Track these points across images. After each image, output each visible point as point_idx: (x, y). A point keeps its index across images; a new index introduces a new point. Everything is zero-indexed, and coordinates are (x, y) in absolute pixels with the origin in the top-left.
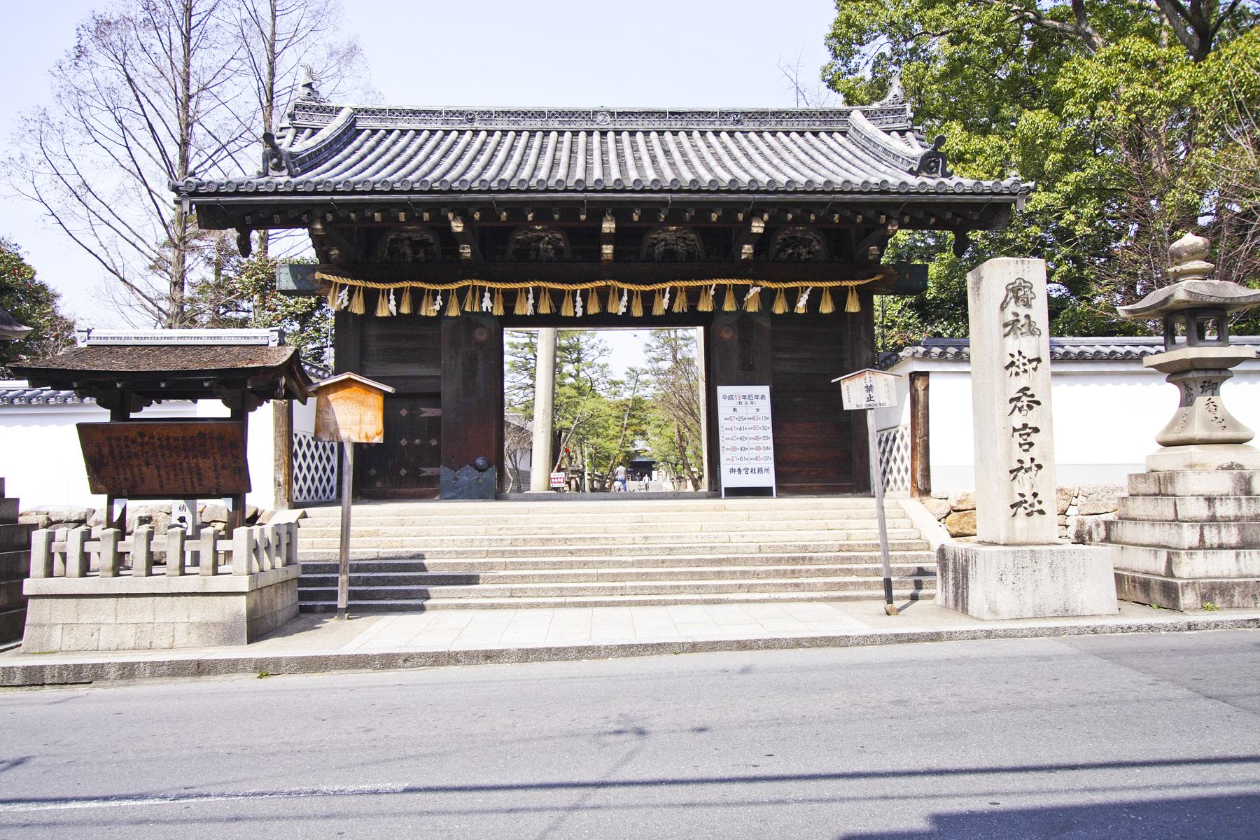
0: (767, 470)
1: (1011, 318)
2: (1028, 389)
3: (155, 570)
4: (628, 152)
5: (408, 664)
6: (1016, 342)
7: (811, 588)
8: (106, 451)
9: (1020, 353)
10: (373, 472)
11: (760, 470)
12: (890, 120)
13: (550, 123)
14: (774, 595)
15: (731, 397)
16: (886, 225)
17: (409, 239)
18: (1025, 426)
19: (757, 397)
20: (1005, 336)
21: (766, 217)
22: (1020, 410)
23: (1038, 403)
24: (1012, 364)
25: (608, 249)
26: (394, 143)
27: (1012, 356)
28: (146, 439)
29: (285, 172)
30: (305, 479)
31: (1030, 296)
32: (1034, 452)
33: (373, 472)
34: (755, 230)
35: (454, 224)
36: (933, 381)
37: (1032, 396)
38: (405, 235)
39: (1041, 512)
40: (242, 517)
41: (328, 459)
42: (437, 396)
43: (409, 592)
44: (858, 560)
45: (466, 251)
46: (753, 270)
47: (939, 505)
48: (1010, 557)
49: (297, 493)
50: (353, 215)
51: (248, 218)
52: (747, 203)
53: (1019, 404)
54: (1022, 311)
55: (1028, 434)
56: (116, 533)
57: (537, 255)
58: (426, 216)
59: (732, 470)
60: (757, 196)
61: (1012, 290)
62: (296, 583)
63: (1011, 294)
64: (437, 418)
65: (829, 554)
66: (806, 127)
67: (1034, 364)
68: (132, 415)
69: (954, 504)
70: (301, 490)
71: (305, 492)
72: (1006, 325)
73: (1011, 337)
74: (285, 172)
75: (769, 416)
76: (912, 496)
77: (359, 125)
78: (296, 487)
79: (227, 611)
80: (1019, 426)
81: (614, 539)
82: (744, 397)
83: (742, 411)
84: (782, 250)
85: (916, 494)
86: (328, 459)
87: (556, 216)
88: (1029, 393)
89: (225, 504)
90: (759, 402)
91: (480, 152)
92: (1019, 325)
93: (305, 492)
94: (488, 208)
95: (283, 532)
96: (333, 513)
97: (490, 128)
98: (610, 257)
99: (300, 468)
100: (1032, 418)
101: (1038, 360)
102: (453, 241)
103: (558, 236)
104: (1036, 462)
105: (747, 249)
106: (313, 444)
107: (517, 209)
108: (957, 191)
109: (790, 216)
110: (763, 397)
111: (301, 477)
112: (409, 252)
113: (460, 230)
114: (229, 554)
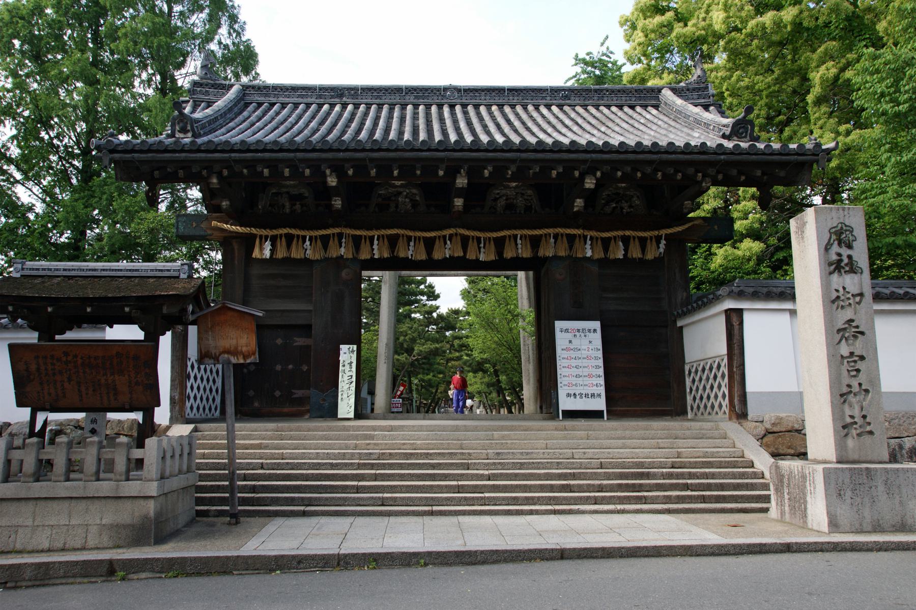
0: (599, 395)
1: (835, 258)
2: (852, 321)
3: (72, 476)
4: (475, 120)
5: (302, 566)
6: (841, 279)
7: (654, 500)
8: (33, 367)
9: (844, 288)
10: (251, 393)
11: (593, 395)
12: (695, 97)
13: (407, 97)
14: (619, 507)
15: (567, 331)
16: (701, 182)
17: (288, 193)
18: (852, 354)
19: (589, 331)
20: (831, 273)
21: (599, 174)
22: (846, 339)
23: (862, 333)
24: (838, 297)
25: (459, 202)
26: (278, 114)
27: (837, 291)
28: (69, 358)
29: (190, 135)
30: (195, 398)
31: (851, 238)
32: (862, 378)
33: (251, 393)
34: (587, 186)
35: (329, 179)
36: (747, 317)
37: (857, 327)
38: (284, 190)
39: (871, 433)
40: (148, 429)
41: (214, 381)
42: (308, 327)
43: (293, 499)
44: (647, 476)
45: (337, 203)
46: (587, 220)
47: (756, 427)
48: (848, 475)
49: (189, 410)
50: (245, 171)
51: (156, 173)
52: (585, 161)
53: (847, 335)
54: (845, 252)
55: (855, 362)
56: (38, 443)
57: (397, 207)
58: (307, 172)
59: (569, 395)
60: (594, 155)
61: (835, 233)
62: (193, 489)
63: (834, 237)
64: (308, 347)
65: (664, 470)
66: (623, 102)
67: (858, 299)
68: (57, 337)
69: (768, 426)
70: (192, 408)
71: (195, 409)
72: (830, 264)
73: (836, 275)
74: (190, 135)
75: (600, 347)
76: (730, 419)
77: (248, 99)
78: (188, 405)
79: (137, 514)
80: (846, 354)
81: (469, 454)
82: (578, 331)
83: (576, 342)
84: (607, 203)
85: (734, 416)
86: (214, 381)
87: (418, 172)
88: (854, 324)
89: (138, 416)
90: (591, 335)
91: (351, 120)
92: (843, 264)
93: (195, 409)
94: (361, 167)
95: (185, 443)
96: (219, 429)
97: (356, 101)
98: (461, 208)
99: (192, 388)
100: (859, 347)
101: (861, 295)
102: (325, 193)
103: (414, 191)
104: (863, 387)
105: (579, 203)
106: (196, 366)
107: (385, 167)
108: (766, 152)
109: (619, 174)
110: (595, 331)
111: (192, 396)
112: (287, 205)
113: (334, 184)
114: (140, 463)
